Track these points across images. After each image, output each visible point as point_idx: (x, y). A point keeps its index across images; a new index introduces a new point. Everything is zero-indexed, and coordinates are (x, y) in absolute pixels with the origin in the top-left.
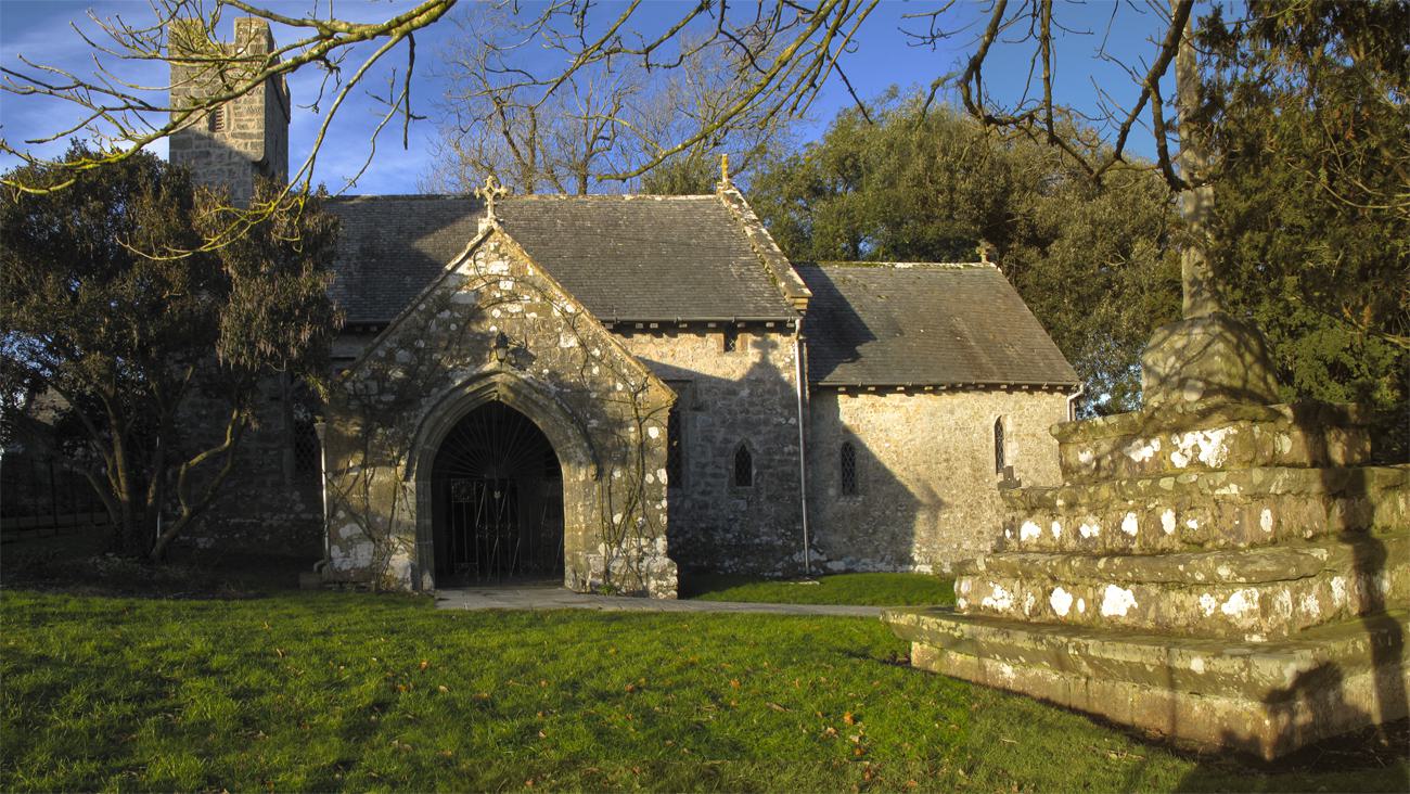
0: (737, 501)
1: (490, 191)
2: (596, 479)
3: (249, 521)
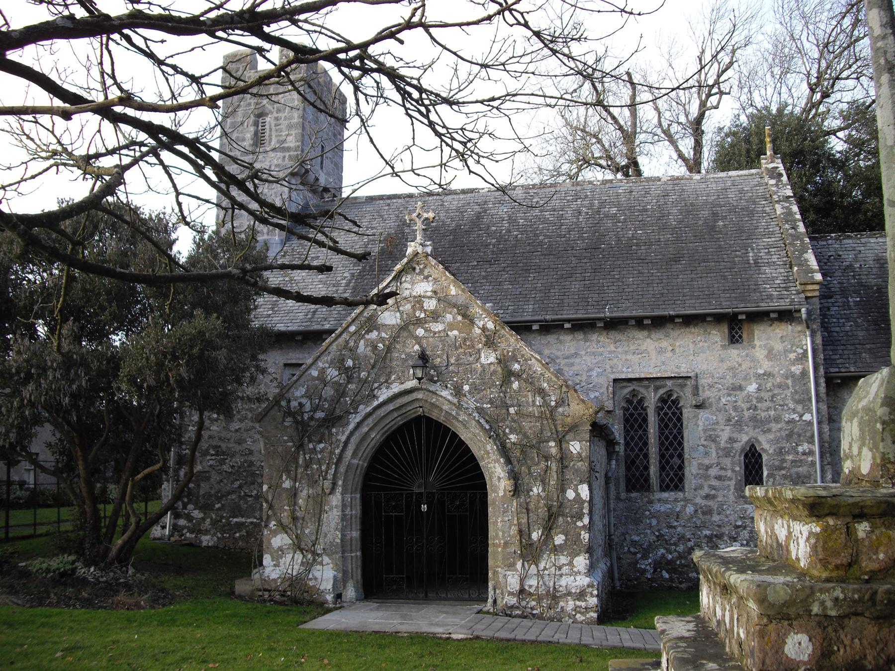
0: (746, 506)
1: (419, 216)
2: (513, 495)
3: (249, 520)
